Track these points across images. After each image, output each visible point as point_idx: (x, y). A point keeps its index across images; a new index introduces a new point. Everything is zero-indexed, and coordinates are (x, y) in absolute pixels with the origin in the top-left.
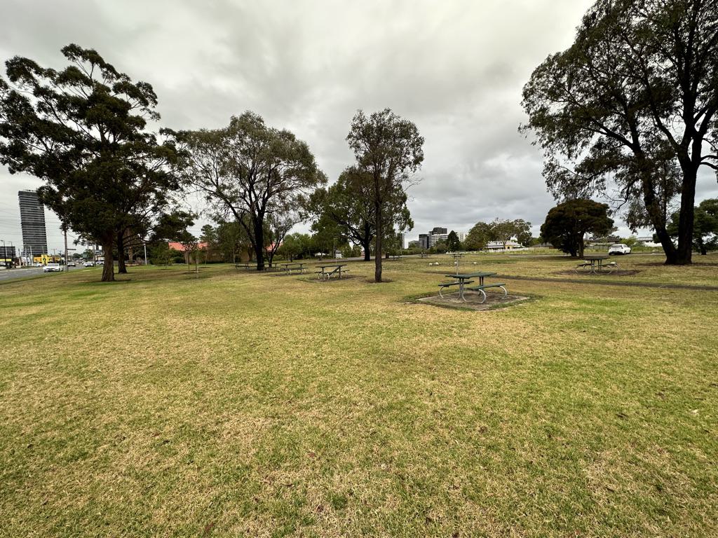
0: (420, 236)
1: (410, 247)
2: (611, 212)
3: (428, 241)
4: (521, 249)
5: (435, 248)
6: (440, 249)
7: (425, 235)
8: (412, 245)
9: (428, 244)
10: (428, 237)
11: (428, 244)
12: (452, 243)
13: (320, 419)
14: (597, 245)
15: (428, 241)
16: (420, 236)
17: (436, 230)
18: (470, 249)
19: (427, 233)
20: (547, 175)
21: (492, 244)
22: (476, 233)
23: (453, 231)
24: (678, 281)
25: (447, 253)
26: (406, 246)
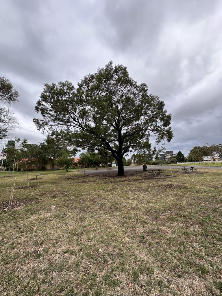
10: (164, 155)
21: (205, 158)
22: (195, 152)
25: (177, 163)
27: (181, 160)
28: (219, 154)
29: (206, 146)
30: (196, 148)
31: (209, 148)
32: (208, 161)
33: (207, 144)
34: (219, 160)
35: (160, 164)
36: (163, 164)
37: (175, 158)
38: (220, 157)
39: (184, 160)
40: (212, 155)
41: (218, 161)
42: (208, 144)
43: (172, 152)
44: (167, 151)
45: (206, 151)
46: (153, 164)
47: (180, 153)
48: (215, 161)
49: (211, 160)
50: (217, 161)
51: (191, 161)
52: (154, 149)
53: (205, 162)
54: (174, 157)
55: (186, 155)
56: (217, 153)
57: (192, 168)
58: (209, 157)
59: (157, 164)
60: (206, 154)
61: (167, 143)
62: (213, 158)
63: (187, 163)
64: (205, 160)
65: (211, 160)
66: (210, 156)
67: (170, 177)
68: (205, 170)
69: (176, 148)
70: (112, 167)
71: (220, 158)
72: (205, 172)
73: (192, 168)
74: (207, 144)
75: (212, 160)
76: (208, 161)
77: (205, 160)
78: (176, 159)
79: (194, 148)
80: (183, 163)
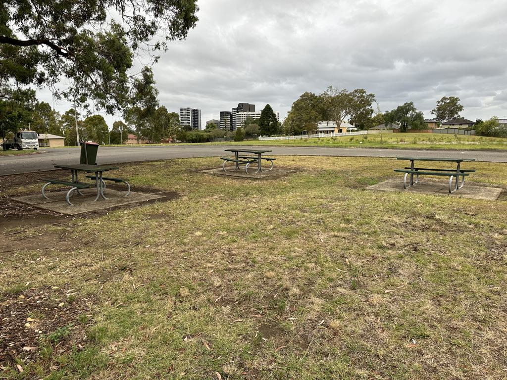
0: (222, 114)
1: (207, 127)
2: (136, 80)
3: (231, 121)
4: (356, 133)
5: (243, 130)
6: (251, 132)
7: (228, 113)
8: (210, 125)
9: (231, 125)
10: (231, 116)
11: (231, 125)
12: (267, 123)
13: (349, 267)
14: (449, 128)
15: (231, 121)
16: (222, 114)
17: (241, 107)
18: (297, 131)
19: (231, 110)
20: (118, 8)
21: (323, 125)
22: (301, 108)
23: (254, 105)
24: (442, 177)
25: (260, 138)
26: (203, 127)
27: (269, 130)
28: (352, 116)
29: (329, 93)
30: (306, 95)
31: (333, 99)
32: (327, 132)
33: (331, 87)
34: (348, 131)
35: (217, 141)
36: (226, 139)
37: (255, 124)
38: (353, 125)
39: (276, 130)
40: (337, 119)
41: (347, 134)
42: (333, 88)
43: (251, 108)
44: (239, 105)
45: (325, 107)
46: (194, 141)
47: (268, 111)
48: (340, 134)
49: (333, 131)
50: (344, 132)
51: (296, 134)
52: (145, 76)
53: (320, 135)
54: (254, 123)
55: (282, 114)
56: (347, 113)
57: (260, 154)
58: (331, 124)
59: (208, 140)
60: (326, 117)
61: (176, 45)
62: (339, 125)
63: (282, 138)
64: (321, 132)
65: (333, 131)
66: (333, 120)
67: (144, 197)
68: (300, 160)
69: (260, 96)
70: (20, 149)
71: (351, 126)
72: (297, 170)
73: (236, 152)
74: (331, 87)
75: (336, 130)
76: (327, 132)
77: (321, 132)
78: (257, 127)
79: (302, 96)
80: (272, 138)
